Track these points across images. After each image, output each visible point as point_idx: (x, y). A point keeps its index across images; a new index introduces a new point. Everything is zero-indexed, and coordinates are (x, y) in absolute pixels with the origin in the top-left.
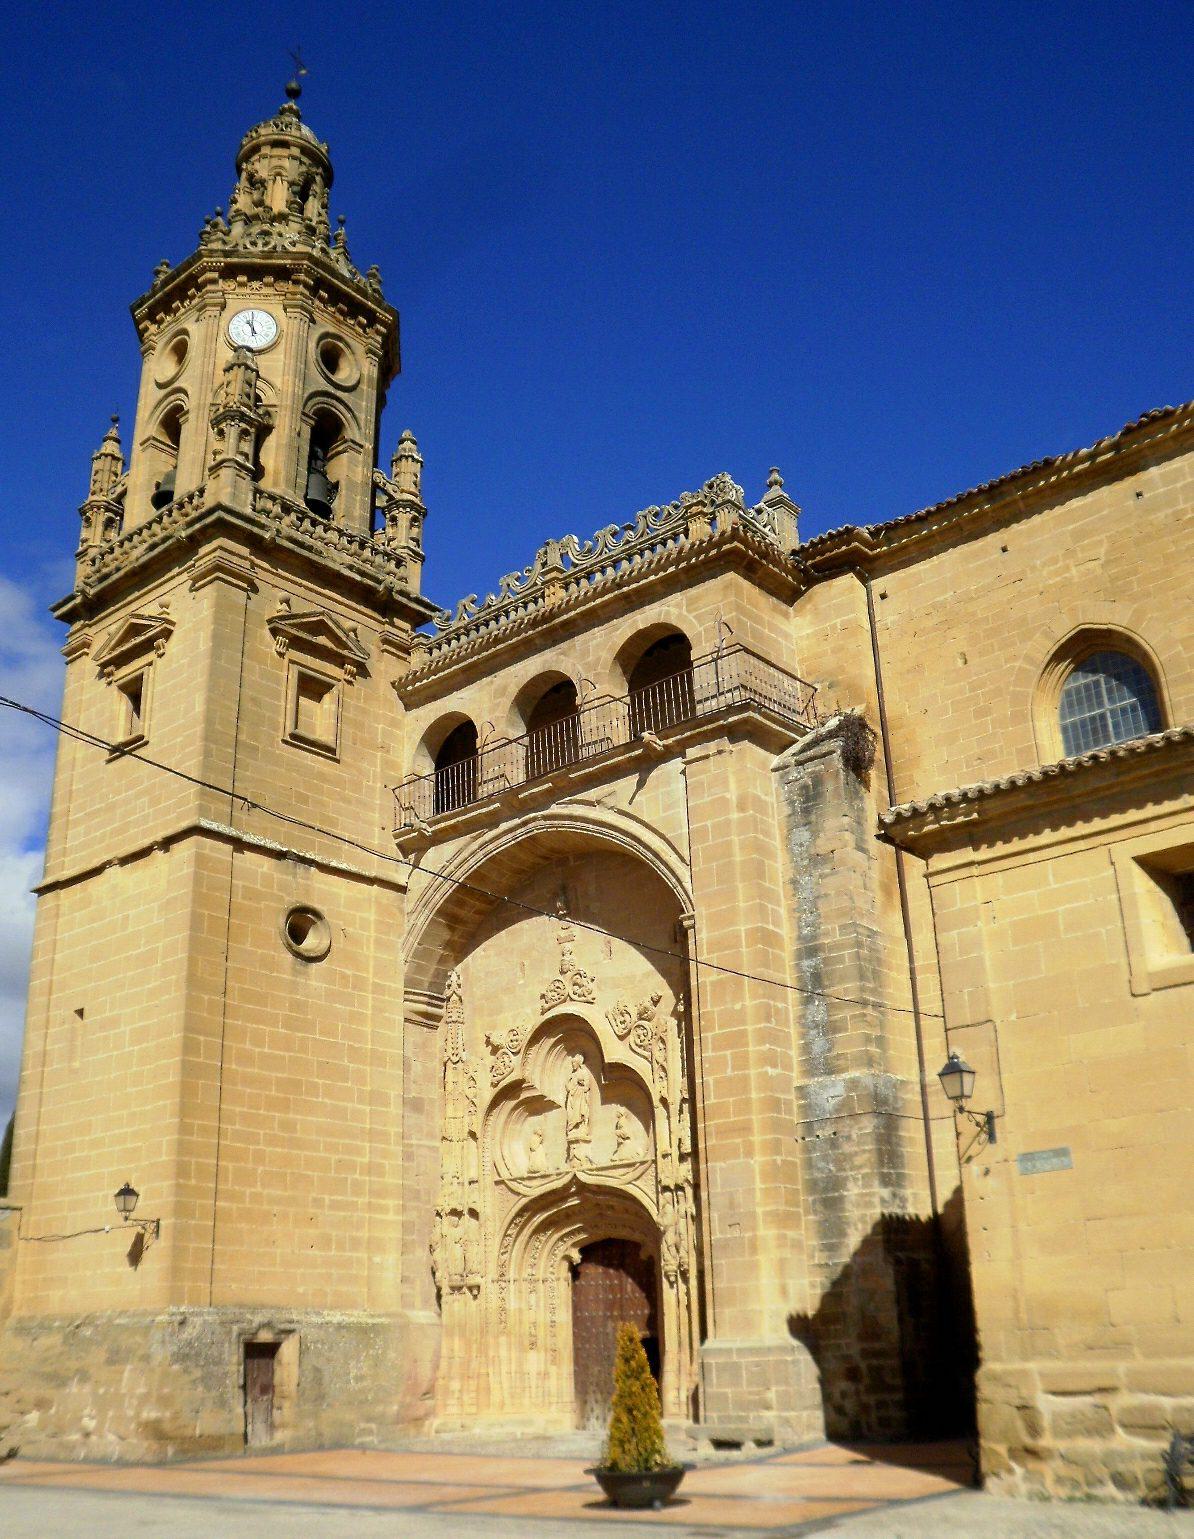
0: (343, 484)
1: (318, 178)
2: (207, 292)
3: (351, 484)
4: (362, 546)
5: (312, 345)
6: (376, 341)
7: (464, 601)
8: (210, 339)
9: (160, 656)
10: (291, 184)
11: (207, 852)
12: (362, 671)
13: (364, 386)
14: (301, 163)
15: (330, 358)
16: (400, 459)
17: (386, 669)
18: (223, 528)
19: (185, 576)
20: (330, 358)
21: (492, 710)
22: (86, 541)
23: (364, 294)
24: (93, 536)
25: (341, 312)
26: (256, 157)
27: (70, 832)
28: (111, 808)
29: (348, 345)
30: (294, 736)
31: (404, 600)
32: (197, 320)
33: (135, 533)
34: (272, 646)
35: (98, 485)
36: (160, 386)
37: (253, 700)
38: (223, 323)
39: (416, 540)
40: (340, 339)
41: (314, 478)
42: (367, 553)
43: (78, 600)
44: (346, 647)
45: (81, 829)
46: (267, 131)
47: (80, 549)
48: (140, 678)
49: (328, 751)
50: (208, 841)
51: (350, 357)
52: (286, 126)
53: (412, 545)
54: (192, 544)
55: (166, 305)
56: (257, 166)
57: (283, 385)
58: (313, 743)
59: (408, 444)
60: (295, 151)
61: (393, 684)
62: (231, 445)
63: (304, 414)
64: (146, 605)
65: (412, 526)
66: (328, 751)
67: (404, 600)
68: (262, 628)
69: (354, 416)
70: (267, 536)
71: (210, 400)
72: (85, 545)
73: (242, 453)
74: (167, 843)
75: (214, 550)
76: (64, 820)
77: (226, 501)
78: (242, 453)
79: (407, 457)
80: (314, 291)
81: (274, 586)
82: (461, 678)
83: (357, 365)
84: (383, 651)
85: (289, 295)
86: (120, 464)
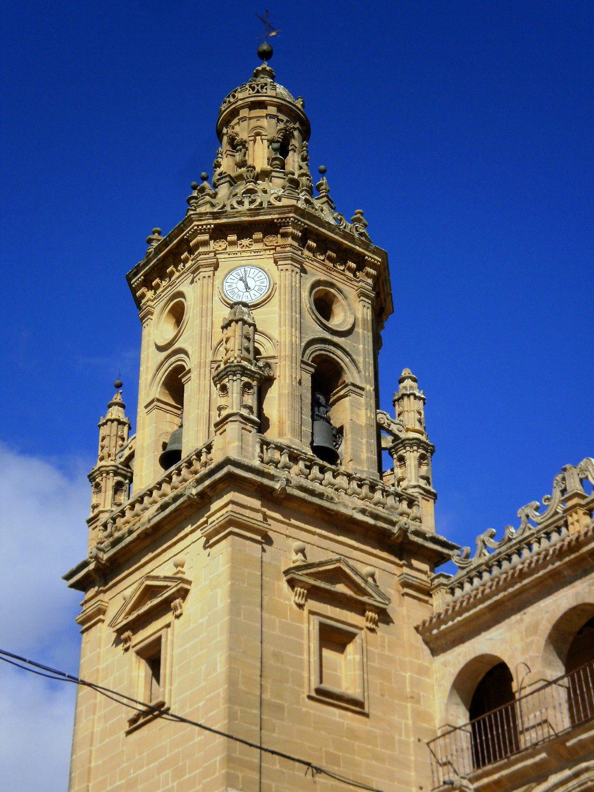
1: (296, 133)
3: (355, 426)
4: (373, 488)
5: (305, 294)
6: (367, 284)
7: (482, 537)
8: (206, 299)
9: (178, 617)
10: (271, 142)
13: (359, 330)
15: (324, 305)
16: (402, 397)
17: (409, 613)
18: (233, 482)
19: (198, 533)
20: (324, 305)
21: (525, 651)
23: (351, 239)
25: (330, 259)
26: (236, 121)
29: (340, 291)
30: (319, 691)
31: (420, 541)
32: (192, 282)
34: (290, 597)
35: (106, 451)
36: (160, 349)
38: (217, 283)
39: (423, 477)
40: (332, 285)
42: (378, 495)
43: (92, 566)
44: (364, 593)
46: (244, 95)
49: (356, 705)
51: (343, 302)
53: (422, 483)
54: (204, 500)
55: (160, 271)
57: (281, 335)
60: (272, 110)
61: (417, 629)
64: (161, 566)
65: (420, 464)
66: (356, 705)
67: (420, 541)
68: (279, 579)
69: (353, 361)
70: (277, 486)
71: (210, 359)
72: (96, 511)
73: (246, 407)
75: (226, 505)
77: (234, 456)
78: (246, 407)
79: (409, 396)
83: (350, 309)
84: (403, 595)
85: (278, 249)
86: (126, 428)
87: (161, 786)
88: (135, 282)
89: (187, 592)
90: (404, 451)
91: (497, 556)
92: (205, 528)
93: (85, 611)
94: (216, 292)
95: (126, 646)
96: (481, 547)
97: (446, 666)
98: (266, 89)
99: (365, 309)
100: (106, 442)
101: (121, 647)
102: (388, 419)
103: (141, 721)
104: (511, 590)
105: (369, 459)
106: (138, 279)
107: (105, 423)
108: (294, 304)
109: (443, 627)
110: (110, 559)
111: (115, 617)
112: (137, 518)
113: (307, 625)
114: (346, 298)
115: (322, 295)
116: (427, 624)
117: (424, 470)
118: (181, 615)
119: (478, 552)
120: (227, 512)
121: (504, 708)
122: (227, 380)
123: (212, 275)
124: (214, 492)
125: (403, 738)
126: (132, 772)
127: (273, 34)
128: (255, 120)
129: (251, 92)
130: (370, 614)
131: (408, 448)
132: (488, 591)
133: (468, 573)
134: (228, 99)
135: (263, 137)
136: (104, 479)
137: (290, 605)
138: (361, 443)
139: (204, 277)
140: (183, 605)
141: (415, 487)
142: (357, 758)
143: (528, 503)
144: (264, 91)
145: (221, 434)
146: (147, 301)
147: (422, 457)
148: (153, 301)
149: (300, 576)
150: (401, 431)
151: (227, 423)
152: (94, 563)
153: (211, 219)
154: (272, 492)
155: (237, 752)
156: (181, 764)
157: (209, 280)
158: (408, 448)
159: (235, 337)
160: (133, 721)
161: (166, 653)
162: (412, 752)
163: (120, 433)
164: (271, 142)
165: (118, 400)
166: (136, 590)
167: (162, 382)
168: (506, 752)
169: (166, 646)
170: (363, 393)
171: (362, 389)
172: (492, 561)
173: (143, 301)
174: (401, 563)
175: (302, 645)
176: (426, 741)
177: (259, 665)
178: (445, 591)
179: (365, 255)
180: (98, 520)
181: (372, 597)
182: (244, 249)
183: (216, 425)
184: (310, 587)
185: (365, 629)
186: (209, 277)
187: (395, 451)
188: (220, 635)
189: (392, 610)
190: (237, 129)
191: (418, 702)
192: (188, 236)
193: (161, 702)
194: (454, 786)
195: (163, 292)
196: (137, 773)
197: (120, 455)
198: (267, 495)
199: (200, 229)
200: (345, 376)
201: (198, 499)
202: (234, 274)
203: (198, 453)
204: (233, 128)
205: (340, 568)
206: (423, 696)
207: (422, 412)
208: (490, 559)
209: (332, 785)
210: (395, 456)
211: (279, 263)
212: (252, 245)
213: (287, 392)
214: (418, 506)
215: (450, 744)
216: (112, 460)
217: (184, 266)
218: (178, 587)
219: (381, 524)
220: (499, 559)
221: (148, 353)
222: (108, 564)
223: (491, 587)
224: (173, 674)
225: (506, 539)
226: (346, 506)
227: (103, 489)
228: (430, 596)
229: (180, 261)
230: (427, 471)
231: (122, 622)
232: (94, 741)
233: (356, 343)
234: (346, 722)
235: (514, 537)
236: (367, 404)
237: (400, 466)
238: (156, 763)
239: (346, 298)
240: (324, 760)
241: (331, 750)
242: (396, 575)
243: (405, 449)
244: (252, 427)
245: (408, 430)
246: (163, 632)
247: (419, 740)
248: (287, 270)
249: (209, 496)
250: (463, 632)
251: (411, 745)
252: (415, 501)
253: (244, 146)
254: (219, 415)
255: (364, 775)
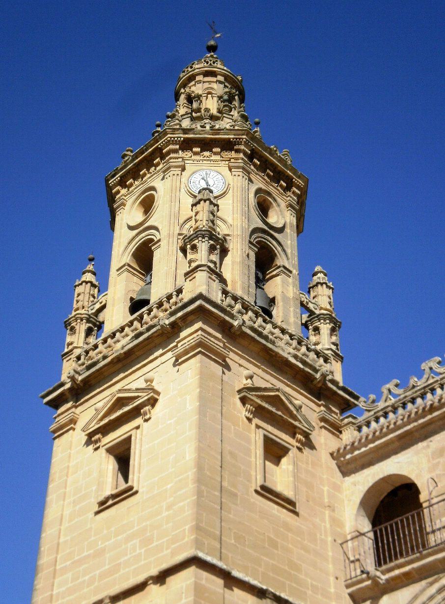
0: (279, 300)
1: (236, 97)
2: (171, 158)
3: (285, 298)
4: (300, 343)
5: (252, 195)
6: (293, 199)
7: (388, 386)
8: (174, 191)
9: (146, 421)
10: (220, 98)
11: (204, 582)
12: (308, 444)
13: (288, 230)
14: (225, 86)
15: (263, 208)
16: (317, 285)
17: (323, 439)
18: (201, 314)
19: (170, 354)
20: (263, 208)
21: (431, 470)
22: (72, 343)
23: (285, 165)
24: (77, 339)
26: (193, 83)
27: (57, 581)
28: (100, 553)
29: (275, 200)
30: (263, 487)
31: (335, 388)
32: (163, 179)
33: (118, 331)
34: (242, 412)
35: (80, 304)
36: (131, 228)
37: (231, 453)
38: (184, 180)
39: (334, 344)
40: (269, 194)
41: (259, 290)
42: (304, 349)
43: (68, 386)
44: (295, 419)
45: (69, 575)
46: (199, 66)
47: (66, 350)
48: (128, 441)
49: (288, 504)
50: (205, 574)
51: (277, 208)
52: (214, 63)
53: (334, 348)
54: (175, 329)
55: (135, 174)
56: (193, 88)
57: (235, 219)
58: (278, 495)
59: (321, 275)
61: (332, 454)
62: (202, 254)
63: (250, 242)
64: (132, 382)
65: (331, 335)
66: (288, 504)
69: (284, 250)
70: (236, 323)
71: (177, 231)
72: (71, 347)
73: (211, 261)
74: (161, 578)
75: (196, 331)
76: (52, 569)
77: (204, 293)
78: (211, 261)
79: (322, 284)
80: (251, 157)
81: (240, 365)
82: (397, 444)
83: (282, 214)
84: (321, 428)
85: (232, 160)
86: (96, 290)
87: (129, 552)
88: (113, 181)
89: (156, 400)
90: (319, 323)
91: (402, 400)
92: (175, 350)
93: (58, 421)
94: (183, 186)
95: (96, 446)
96: (387, 394)
97: (355, 485)
98: (217, 64)
99: (292, 217)
100: (81, 298)
101: (91, 447)
102: (306, 299)
103: (110, 502)
104: (421, 421)
105: (295, 323)
106: (115, 180)
107: (81, 284)
108: (244, 199)
109: (357, 453)
110: (83, 381)
111: (88, 423)
112: (110, 349)
113: (254, 435)
114: (279, 205)
115: (261, 200)
116: (341, 451)
117: (334, 339)
118: (150, 418)
119: (384, 398)
120: (198, 336)
121: (406, 518)
122: (197, 241)
123: (180, 174)
124: (184, 322)
125: (323, 537)
126: (100, 544)
127: (218, 35)
128: (208, 83)
129: (205, 64)
130: (299, 436)
131: (322, 321)
132: (399, 422)
133: (375, 413)
134: (186, 70)
135: (213, 95)
136: (78, 324)
137: (242, 417)
138: (290, 311)
139: (174, 175)
140: (152, 411)
141: (328, 349)
142: (290, 546)
143: (431, 358)
144: (215, 65)
145: (190, 281)
146: (122, 196)
147: (333, 330)
148: (125, 196)
149: (252, 396)
150: (316, 309)
151: (197, 271)
152: (70, 383)
153: (181, 134)
154: (231, 328)
155: (204, 523)
156: (148, 534)
157: (178, 177)
158: (322, 321)
159: (203, 211)
160: (102, 503)
161: (135, 448)
162: (329, 549)
163: (92, 292)
164: (220, 98)
165: (91, 269)
166: (109, 402)
167: (132, 252)
168: (418, 548)
169: (135, 444)
170: (291, 275)
171: (291, 272)
172: (398, 403)
173: (117, 197)
174: (320, 403)
175: (250, 450)
176: (340, 542)
177: (219, 457)
178: (353, 428)
179: (294, 178)
180: (72, 354)
181: (301, 423)
182: (205, 158)
183: (187, 274)
184: (257, 406)
185: (295, 447)
186: (178, 175)
187: (311, 323)
188: (189, 431)
189: (314, 437)
190: (193, 88)
191: (334, 511)
192: (164, 144)
193: (130, 486)
194: (370, 575)
195: (134, 189)
196: (105, 544)
197: (92, 307)
198: (226, 329)
199: (173, 141)
200: (278, 261)
201: (169, 329)
202: (197, 174)
203: (169, 296)
204: (190, 88)
205: (278, 396)
206: (337, 507)
207: (332, 297)
208: (396, 402)
209: (272, 563)
210: (310, 327)
211: (233, 170)
212: (211, 156)
213: (239, 261)
214: (331, 363)
215: (359, 546)
216: (85, 310)
217: (155, 169)
218: (149, 396)
219: (307, 369)
220: (404, 402)
221: (121, 232)
222: (82, 385)
223: (402, 420)
224: (142, 464)
225: (411, 386)
226: (284, 351)
227: (77, 331)
228: (341, 432)
229: (153, 165)
230: (337, 340)
231: (94, 426)
232: (64, 520)
233: (286, 239)
234: (282, 516)
235: (418, 385)
236: (294, 283)
237: (315, 335)
238: (124, 535)
239: (279, 205)
240: (267, 543)
241: (272, 536)
242: (316, 412)
243: (320, 321)
244: (216, 277)
245: (321, 309)
246: (133, 432)
247: (335, 541)
248: (239, 176)
249: (179, 326)
250: (372, 458)
251: (329, 543)
252: (328, 359)
253: (199, 99)
254: (189, 267)
255: (296, 561)
